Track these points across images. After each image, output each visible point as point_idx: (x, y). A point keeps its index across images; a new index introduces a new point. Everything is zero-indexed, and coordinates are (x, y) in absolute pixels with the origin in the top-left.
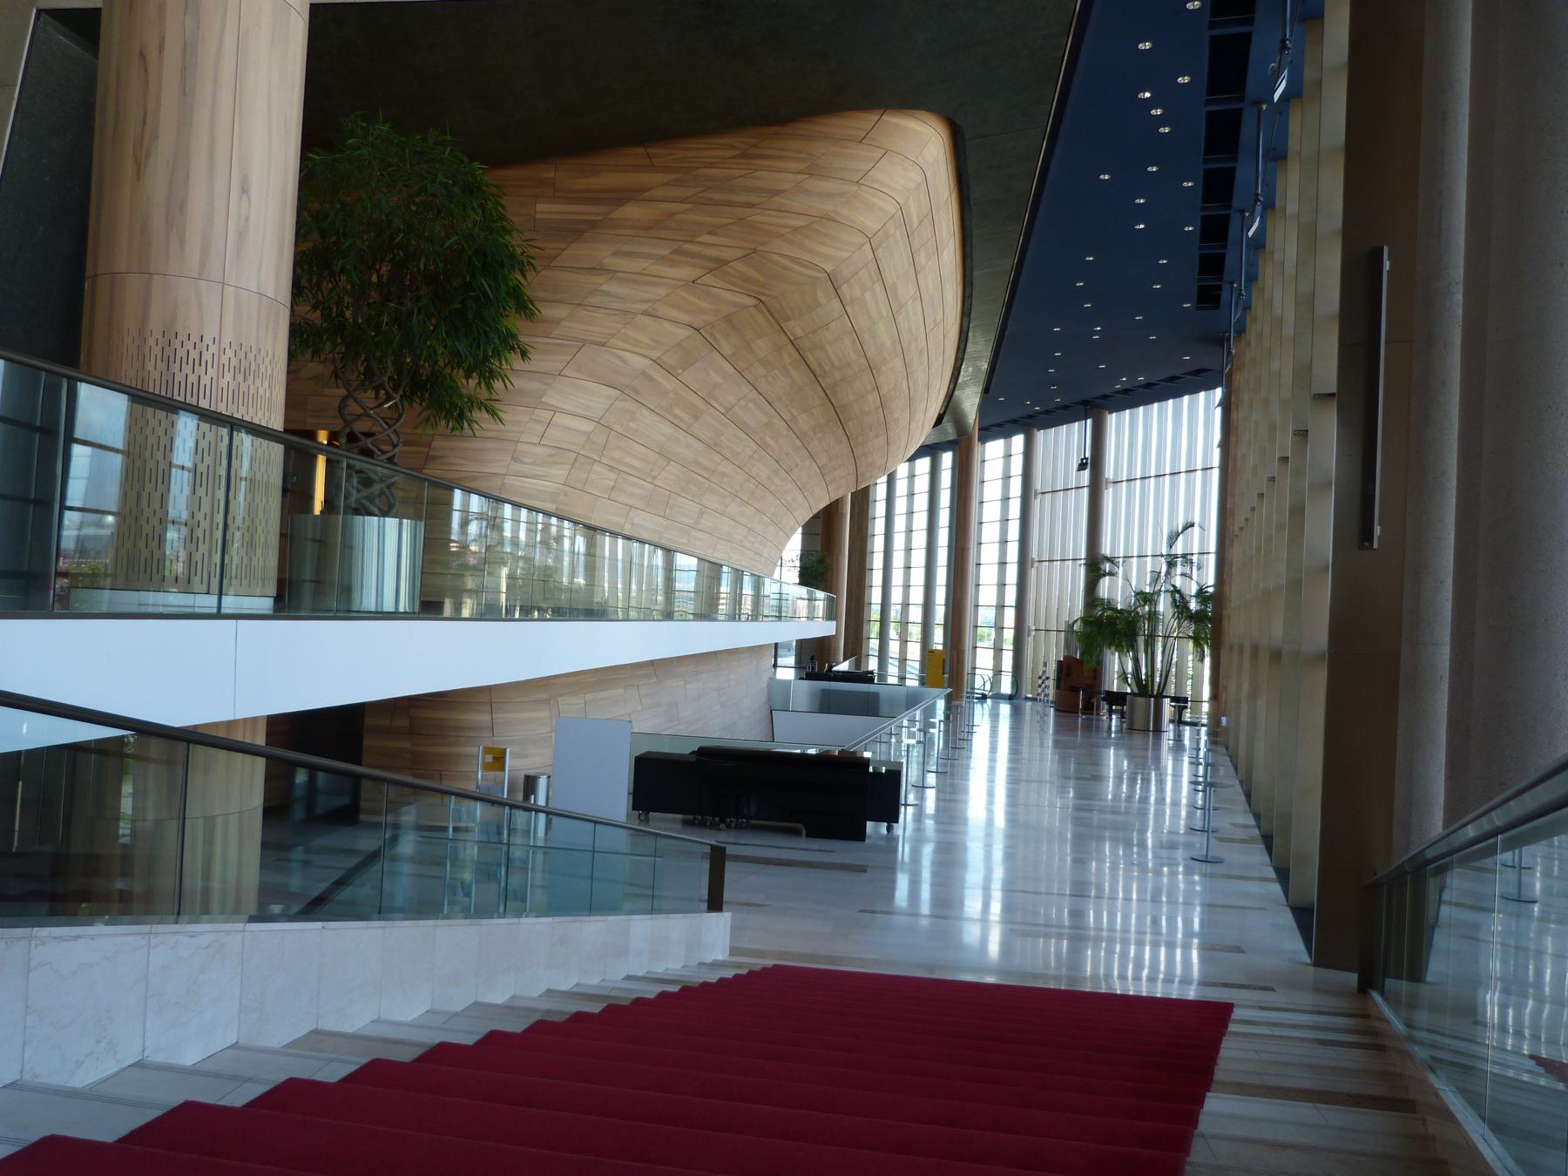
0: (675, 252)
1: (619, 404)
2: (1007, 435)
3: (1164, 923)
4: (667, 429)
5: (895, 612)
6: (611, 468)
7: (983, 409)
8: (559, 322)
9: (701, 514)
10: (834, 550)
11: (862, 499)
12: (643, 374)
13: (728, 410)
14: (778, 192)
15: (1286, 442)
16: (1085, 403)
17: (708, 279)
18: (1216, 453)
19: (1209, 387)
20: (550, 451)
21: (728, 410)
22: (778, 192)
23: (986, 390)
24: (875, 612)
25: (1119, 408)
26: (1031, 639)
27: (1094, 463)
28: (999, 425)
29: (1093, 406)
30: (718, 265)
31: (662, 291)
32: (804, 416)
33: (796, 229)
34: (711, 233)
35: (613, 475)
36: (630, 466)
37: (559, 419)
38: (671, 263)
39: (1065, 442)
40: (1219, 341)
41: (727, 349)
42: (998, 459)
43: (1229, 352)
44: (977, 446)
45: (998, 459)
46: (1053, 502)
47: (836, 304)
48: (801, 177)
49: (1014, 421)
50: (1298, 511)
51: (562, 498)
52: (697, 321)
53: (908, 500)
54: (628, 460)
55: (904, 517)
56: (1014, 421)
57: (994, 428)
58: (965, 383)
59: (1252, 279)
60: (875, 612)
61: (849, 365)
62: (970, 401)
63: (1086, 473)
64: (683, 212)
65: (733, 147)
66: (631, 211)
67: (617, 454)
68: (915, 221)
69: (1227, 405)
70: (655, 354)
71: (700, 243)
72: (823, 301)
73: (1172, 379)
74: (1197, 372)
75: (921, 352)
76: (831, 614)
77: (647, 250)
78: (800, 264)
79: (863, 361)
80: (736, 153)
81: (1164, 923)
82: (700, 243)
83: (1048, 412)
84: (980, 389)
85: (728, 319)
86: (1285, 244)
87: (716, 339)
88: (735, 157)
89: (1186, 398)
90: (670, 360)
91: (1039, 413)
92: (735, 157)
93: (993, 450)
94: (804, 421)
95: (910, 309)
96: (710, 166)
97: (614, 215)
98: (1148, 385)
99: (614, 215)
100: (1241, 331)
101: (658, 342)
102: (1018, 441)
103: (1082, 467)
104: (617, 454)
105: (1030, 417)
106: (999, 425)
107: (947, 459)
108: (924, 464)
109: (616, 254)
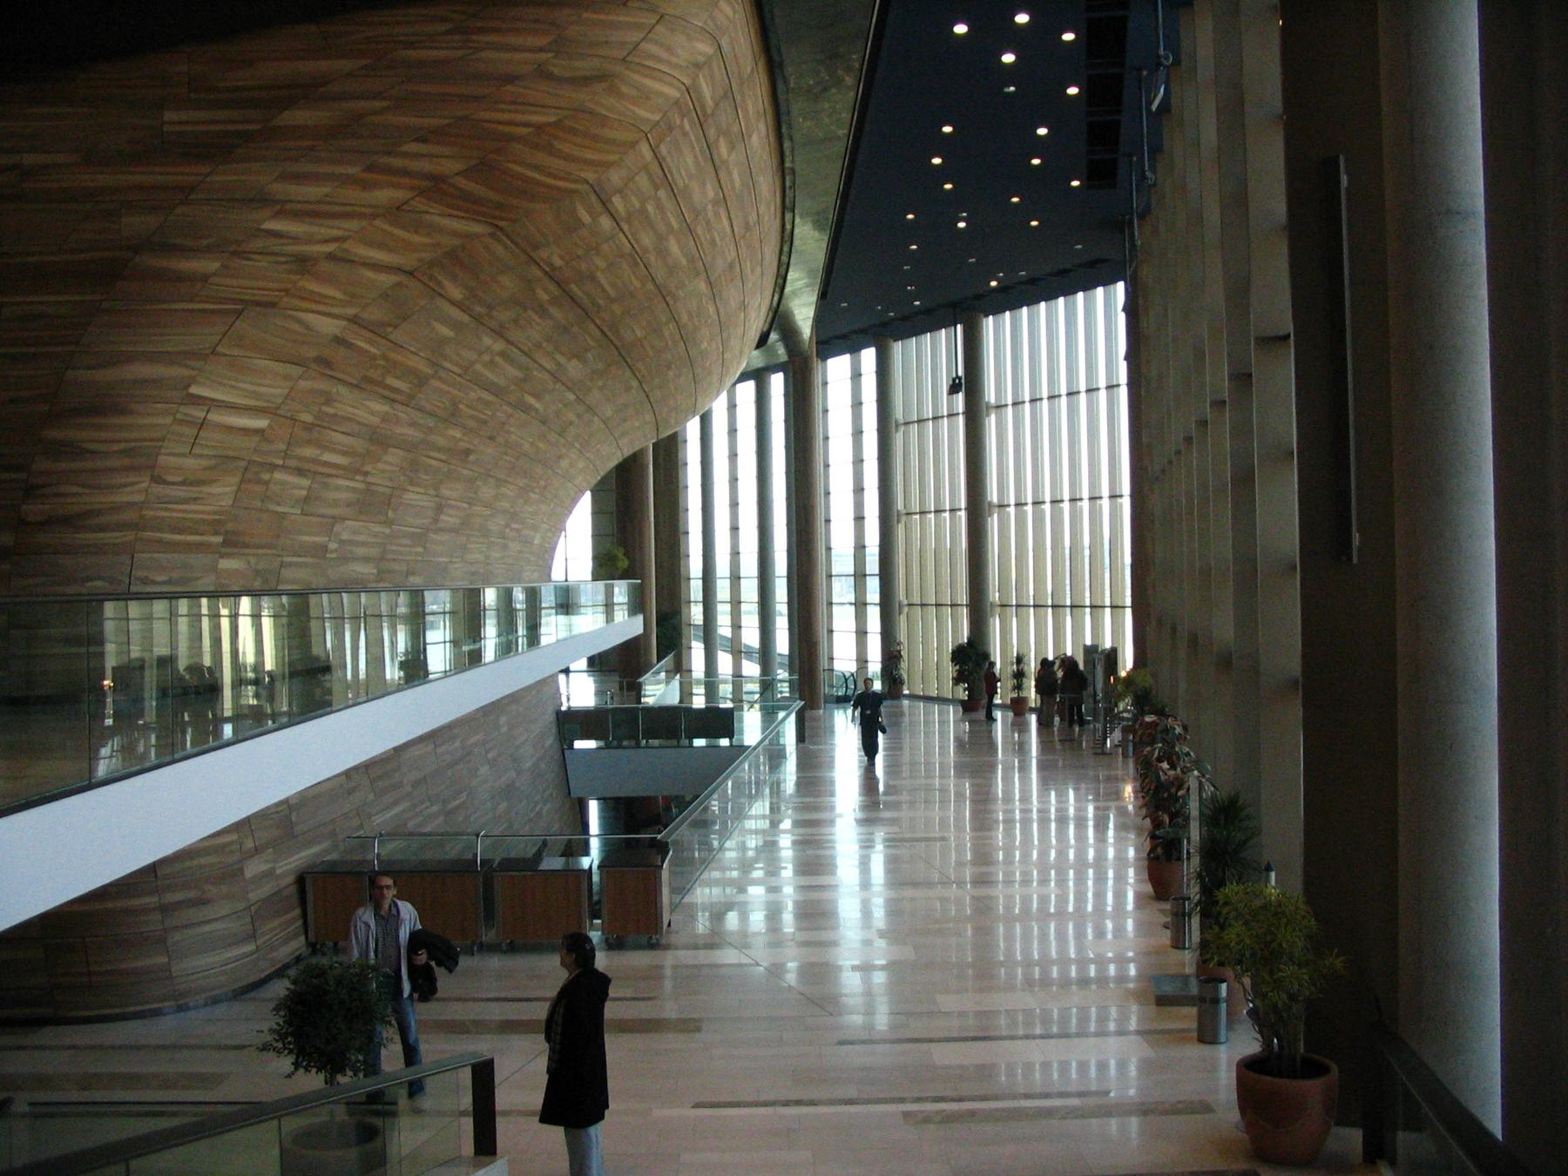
0: (370, 169)
1: (303, 384)
2: (854, 349)
3: (1090, 931)
4: (380, 407)
5: (723, 590)
6: (300, 472)
7: (818, 321)
8: (205, 278)
9: (439, 509)
10: (641, 523)
11: (669, 451)
12: (340, 341)
13: (466, 369)
14: (512, 79)
15: (1218, 379)
16: (953, 305)
17: (419, 204)
18: (1123, 367)
19: (1108, 281)
20: (204, 463)
21: (466, 369)
22: (512, 79)
23: (823, 296)
24: (696, 589)
25: (997, 310)
26: (903, 618)
27: (969, 383)
28: (844, 337)
29: (964, 308)
30: (436, 188)
31: (353, 225)
32: (575, 362)
33: (539, 128)
34: (417, 140)
35: (305, 482)
36: (335, 466)
37: (215, 417)
38: (366, 186)
39: (932, 355)
40: (1119, 226)
41: (456, 293)
42: (844, 380)
43: (1133, 246)
44: (817, 365)
45: (844, 380)
46: (921, 436)
47: (606, 223)
48: (543, 56)
49: (863, 331)
50: (1244, 480)
51: (230, 526)
52: (408, 260)
53: (727, 447)
54: (328, 457)
55: (728, 607)
56: (863, 331)
57: (833, 339)
58: (794, 293)
59: (1156, 149)
60: (696, 589)
61: (631, 295)
62: (804, 314)
63: (960, 397)
64: (376, 113)
65: (444, 20)
66: (299, 116)
67: (308, 452)
68: (709, 102)
69: (1133, 310)
70: (350, 311)
71: (406, 155)
72: (586, 218)
73: (1063, 273)
74: (1093, 264)
75: (731, 266)
76: (637, 605)
77: (325, 168)
78: (550, 175)
79: (650, 286)
80: (448, 26)
81: (1090, 931)
82: (406, 155)
83: (905, 318)
84: (814, 298)
85: (452, 255)
86: (1201, 122)
87: (439, 283)
88: (448, 32)
89: (1080, 295)
90: (374, 314)
91: (893, 319)
92: (448, 32)
93: (837, 368)
94: (574, 369)
95: (710, 214)
96: (411, 45)
97: (278, 122)
98: (1032, 281)
99: (278, 122)
100: (1145, 214)
101: (353, 296)
102: (869, 356)
103: (954, 389)
104: (308, 452)
105: (884, 325)
106: (844, 337)
107: (777, 382)
108: (747, 390)
109: (285, 177)
